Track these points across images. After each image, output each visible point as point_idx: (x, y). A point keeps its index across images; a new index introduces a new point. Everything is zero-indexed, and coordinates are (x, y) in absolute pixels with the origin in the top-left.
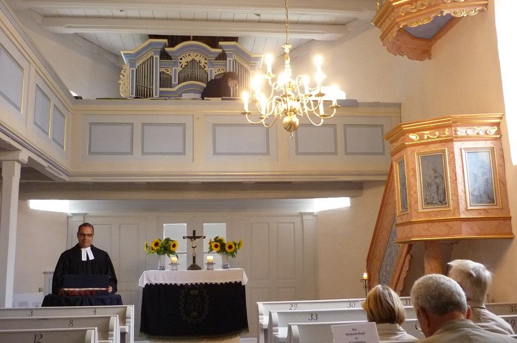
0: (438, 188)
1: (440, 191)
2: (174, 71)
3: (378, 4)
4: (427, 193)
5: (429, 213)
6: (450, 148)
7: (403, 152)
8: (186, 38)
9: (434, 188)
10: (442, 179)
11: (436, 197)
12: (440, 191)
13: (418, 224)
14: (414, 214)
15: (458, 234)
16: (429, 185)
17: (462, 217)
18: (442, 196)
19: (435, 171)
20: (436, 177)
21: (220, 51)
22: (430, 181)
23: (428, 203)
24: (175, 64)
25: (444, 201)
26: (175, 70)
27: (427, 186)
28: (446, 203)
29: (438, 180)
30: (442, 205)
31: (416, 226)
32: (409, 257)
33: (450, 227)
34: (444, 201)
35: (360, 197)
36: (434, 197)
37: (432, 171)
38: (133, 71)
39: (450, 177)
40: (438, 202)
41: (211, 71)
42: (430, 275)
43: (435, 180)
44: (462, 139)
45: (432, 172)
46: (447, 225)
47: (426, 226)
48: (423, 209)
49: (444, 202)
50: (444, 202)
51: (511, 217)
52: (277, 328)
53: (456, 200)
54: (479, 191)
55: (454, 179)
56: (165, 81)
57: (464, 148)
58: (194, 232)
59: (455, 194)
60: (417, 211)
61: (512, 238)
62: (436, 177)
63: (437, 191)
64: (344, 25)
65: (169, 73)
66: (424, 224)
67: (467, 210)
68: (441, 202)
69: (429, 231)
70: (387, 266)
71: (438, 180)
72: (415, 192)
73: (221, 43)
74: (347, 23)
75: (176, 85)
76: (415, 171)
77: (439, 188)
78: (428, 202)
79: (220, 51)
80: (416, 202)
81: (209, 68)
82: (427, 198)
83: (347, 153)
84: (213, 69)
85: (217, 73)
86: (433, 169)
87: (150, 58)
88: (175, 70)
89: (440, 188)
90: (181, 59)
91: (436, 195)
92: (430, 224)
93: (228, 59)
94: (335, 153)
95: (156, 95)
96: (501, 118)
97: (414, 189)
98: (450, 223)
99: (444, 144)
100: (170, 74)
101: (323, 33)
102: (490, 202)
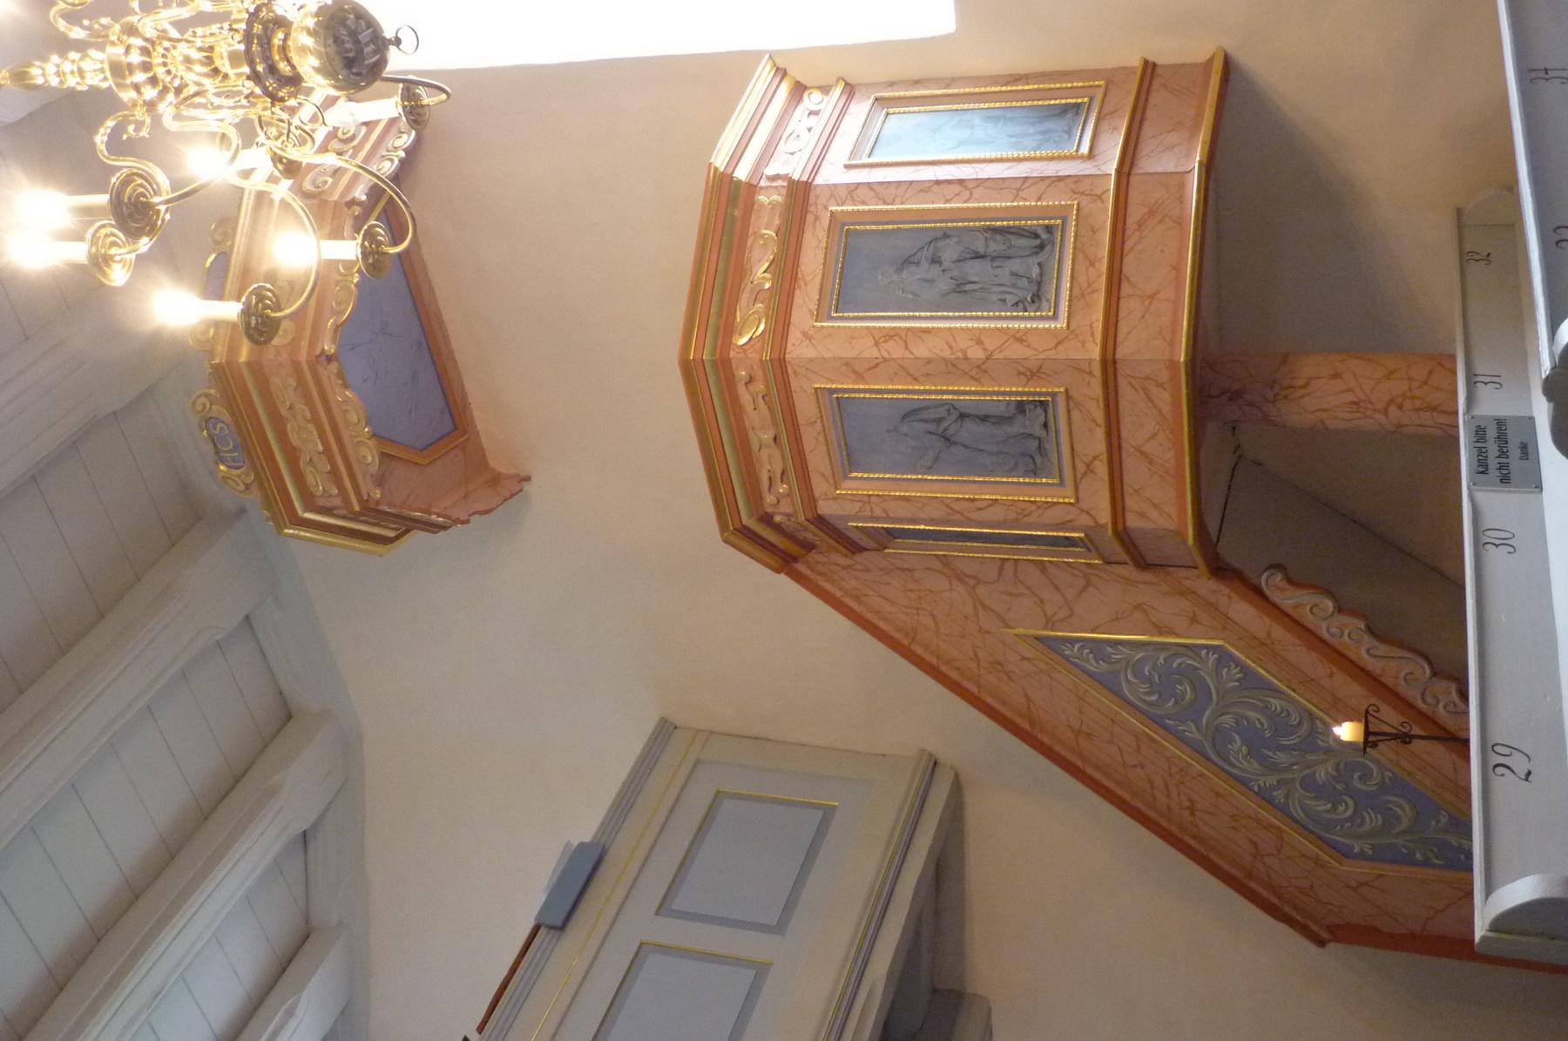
0: (979, 256)
1: (996, 247)
4: (995, 298)
5: (1076, 291)
6: (832, 195)
7: (803, 389)
9: (975, 270)
10: (946, 236)
11: (1016, 265)
12: (996, 247)
13: (1119, 339)
14: (1072, 351)
15: (1182, 186)
17: (1112, 168)
19: (908, 262)
20: (935, 261)
22: (944, 284)
23: (1037, 298)
27: (962, 295)
28: (1049, 229)
29: (949, 253)
30: (1053, 243)
31: (1125, 349)
32: (1273, 584)
33: (1151, 213)
34: (1036, 236)
35: (993, 1029)
36: (1014, 274)
37: (905, 275)
39: (947, 201)
40: (1040, 258)
42: (1370, 764)
43: (946, 264)
44: (817, 167)
45: (912, 275)
46: (1140, 224)
47: (1130, 307)
48: (1062, 483)
49: (1044, 236)
50: (1044, 236)
51: (1146, 63)
53: (1042, 186)
54: (1027, 135)
55: (957, 188)
59: (1018, 190)
60: (1059, 339)
61: (1228, 65)
62: (935, 261)
63: (993, 259)
64: (307, 936)
66: (1123, 311)
67: (1091, 155)
68: (1041, 247)
69: (1152, 297)
70: (1308, 783)
72: (979, 342)
74: (307, 923)
76: (891, 335)
77: (981, 250)
78: (1035, 296)
80: (1020, 337)
82: (1011, 299)
83: (780, 928)
86: (900, 269)
89: (980, 246)
91: (1008, 263)
92: (1126, 289)
94: (761, 971)
96: (781, 73)
97: (963, 343)
98: (1135, 214)
99: (810, 218)
101: (290, 1013)
102: (1077, 113)
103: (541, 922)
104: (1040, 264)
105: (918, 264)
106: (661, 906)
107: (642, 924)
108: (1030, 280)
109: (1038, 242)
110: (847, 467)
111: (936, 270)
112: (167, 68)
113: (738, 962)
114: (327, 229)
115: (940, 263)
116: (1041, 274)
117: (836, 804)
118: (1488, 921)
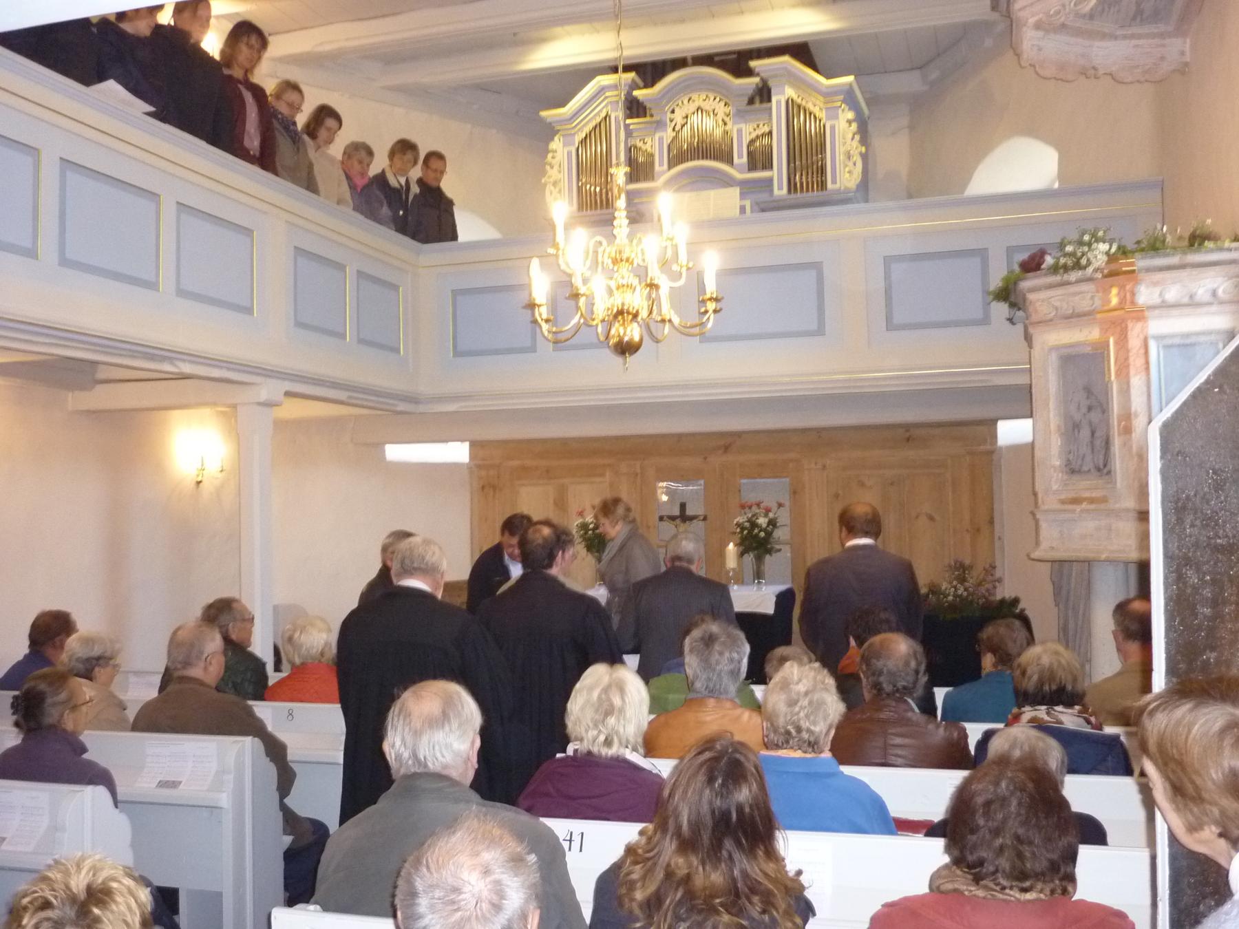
0: (1093, 433)
1: (1098, 443)
2: (655, 144)
3: (401, 213)
8: (678, 63)
9: (1085, 433)
11: (1089, 458)
16: (1076, 426)
18: (1101, 457)
20: (1090, 409)
21: (755, 80)
23: (1073, 472)
24: (660, 125)
25: (1105, 466)
26: (661, 140)
38: (569, 154)
41: (740, 132)
49: (1105, 471)
50: (1105, 471)
52: (105, 898)
56: (639, 170)
57: (1159, 338)
58: (683, 506)
62: (1090, 409)
65: (648, 147)
68: (1099, 470)
71: (1095, 416)
73: (753, 64)
75: (663, 173)
79: (755, 80)
81: (734, 123)
84: (743, 126)
85: (754, 135)
87: (605, 118)
88: (661, 140)
89: (1097, 434)
90: (673, 112)
93: (774, 99)
95: (740, 156)
100: (649, 149)
103: (1087, 699)
104: (1089, 470)
105: (1088, 398)
106: (181, 204)
107: (53, 149)
108: (1081, 466)
109: (1102, 467)
110: (1169, 342)
111: (1084, 410)
112: (620, 69)
113: (157, 275)
114: (401, 688)
115: (1089, 411)
116: (1085, 472)
117: (255, 315)
118: (347, 142)
